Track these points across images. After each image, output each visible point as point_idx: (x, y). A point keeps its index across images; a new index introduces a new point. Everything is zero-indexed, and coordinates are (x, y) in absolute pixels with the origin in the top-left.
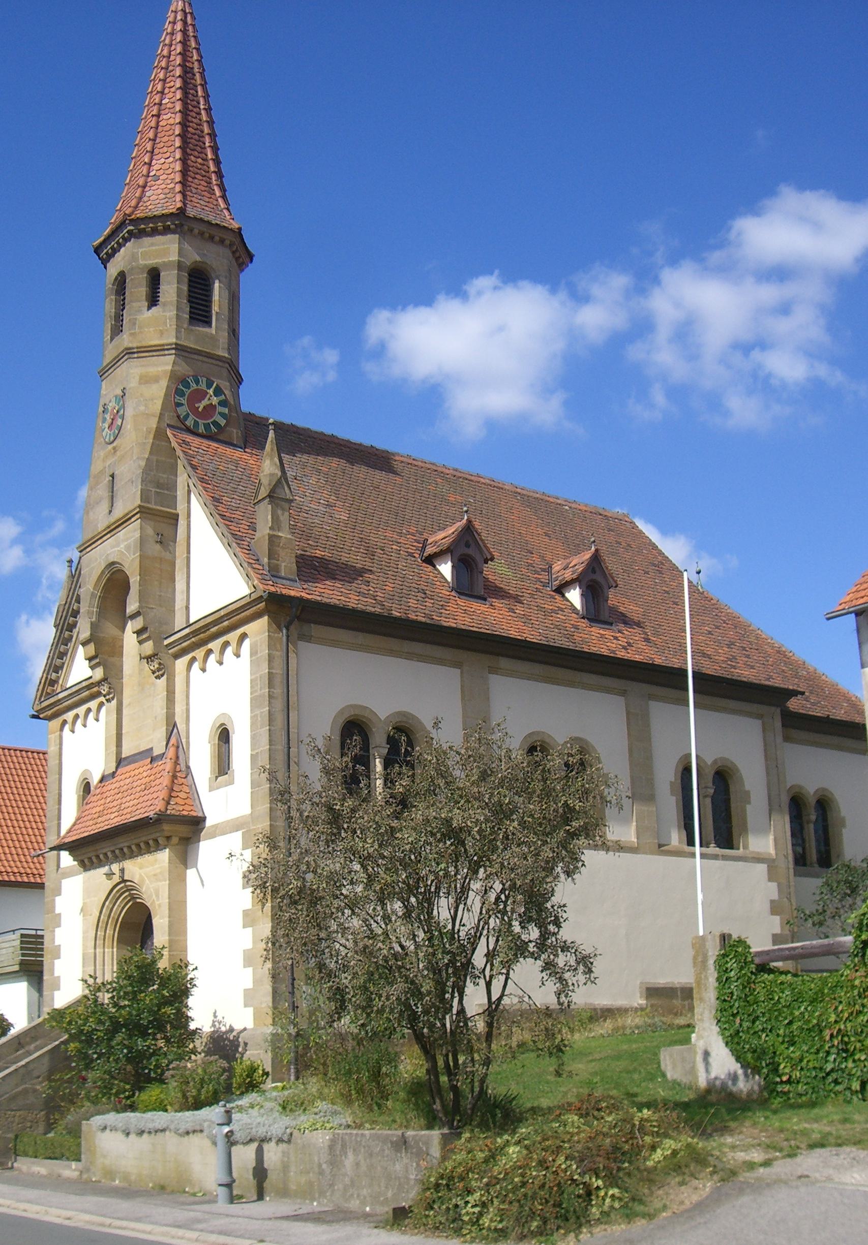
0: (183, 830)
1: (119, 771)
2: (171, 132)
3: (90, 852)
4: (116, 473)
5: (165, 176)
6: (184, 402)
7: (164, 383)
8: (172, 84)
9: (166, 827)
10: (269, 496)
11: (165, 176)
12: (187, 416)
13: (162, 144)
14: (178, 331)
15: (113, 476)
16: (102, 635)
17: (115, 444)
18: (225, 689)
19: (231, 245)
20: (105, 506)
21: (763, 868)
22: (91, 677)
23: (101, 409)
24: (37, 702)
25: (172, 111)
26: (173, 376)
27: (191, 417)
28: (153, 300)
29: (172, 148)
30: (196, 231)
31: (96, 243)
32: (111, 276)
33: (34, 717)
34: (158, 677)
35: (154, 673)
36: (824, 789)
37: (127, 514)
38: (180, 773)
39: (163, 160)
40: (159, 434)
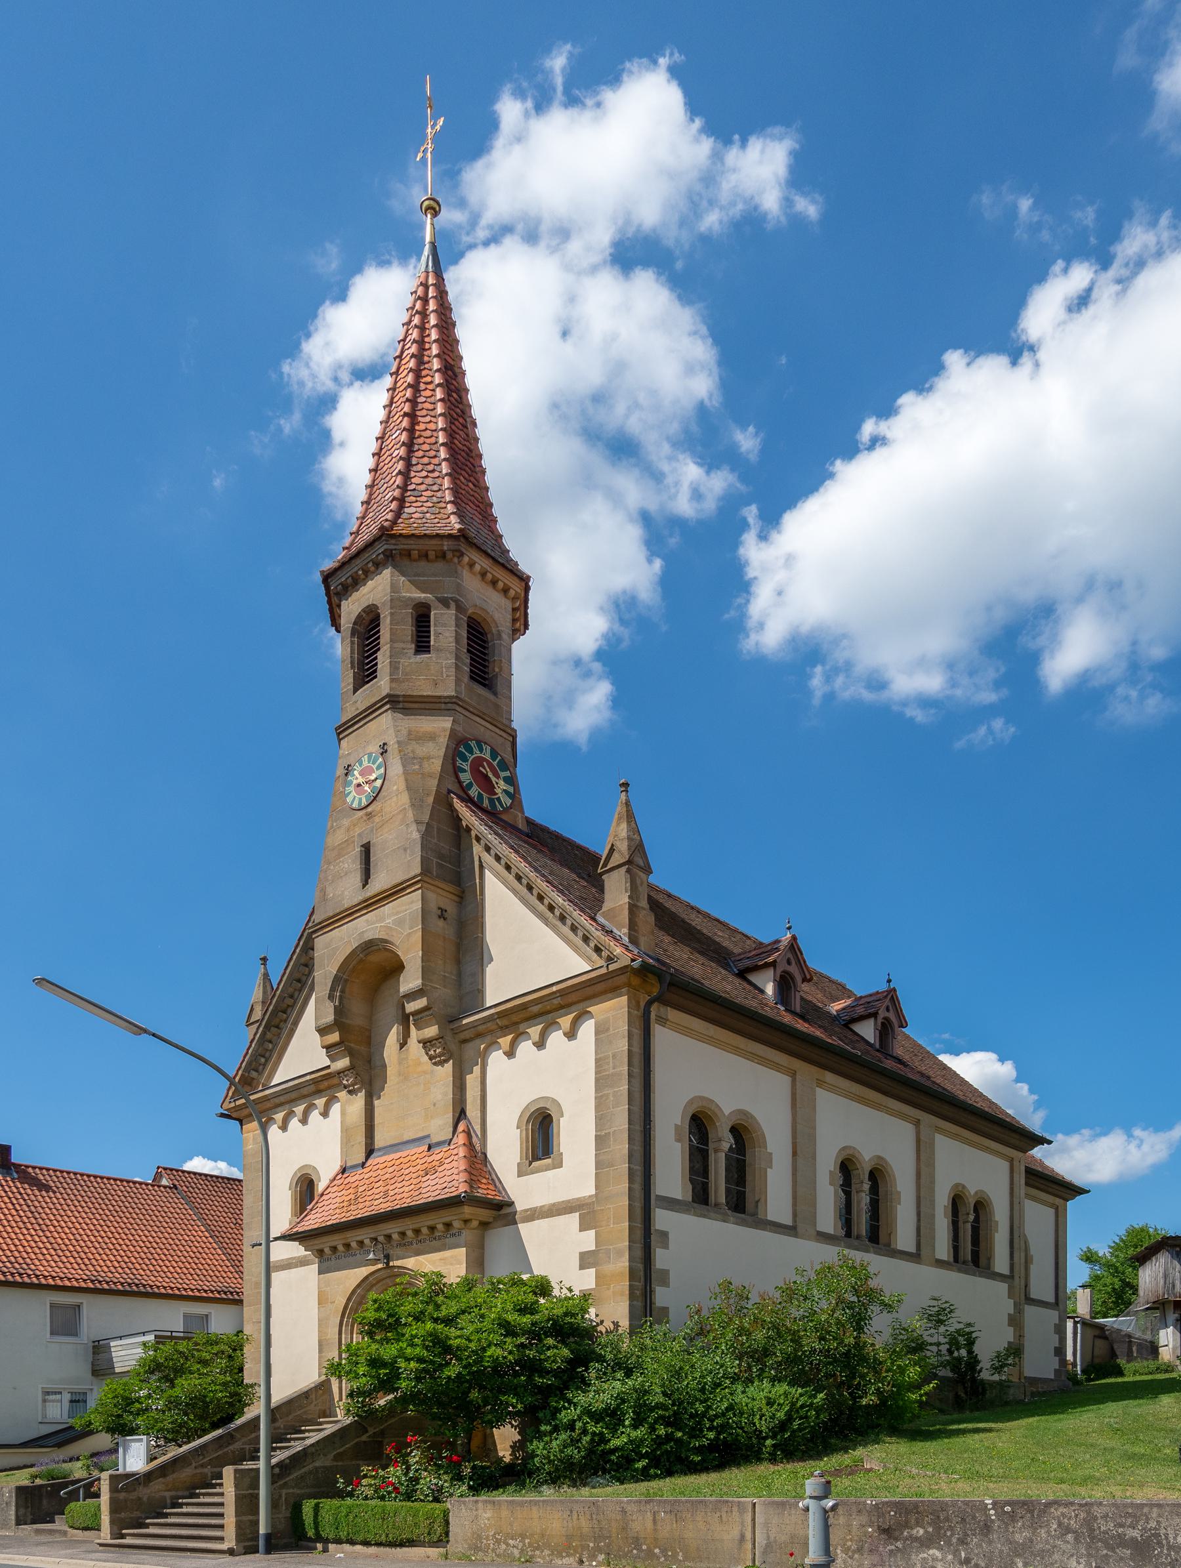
0: (485, 1214)
1: (370, 1162)
2: (433, 440)
3: (326, 1243)
4: (376, 841)
5: (429, 493)
6: (467, 768)
7: (443, 740)
8: (428, 379)
9: (467, 1211)
10: (629, 862)
11: (429, 493)
12: (470, 785)
13: (420, 454)
14: (458, 681)
15: (367, 849)
16: (347, 1021)
17: (369, 809)
18: (565, 1071)
19: (514, 599)
20: (356, 878)
21: (575, 1217)
22: (328, 1067)
23: (340, 771)
24: (228, 1100)
25: (432, 413)
26: (453, 732)
27: (475, 787)
28: (422, 644)
29: (436, 461)
30: (477, 568)
31: (328, 565)
32: (349, 613)
33: (222, 1115)
34: (441, 1063)
35: (431, 1059)
36: (879, 1157)
37: (402, 883)
38: (477, 1162)
39: (424, 474)
40: (443, 801)
